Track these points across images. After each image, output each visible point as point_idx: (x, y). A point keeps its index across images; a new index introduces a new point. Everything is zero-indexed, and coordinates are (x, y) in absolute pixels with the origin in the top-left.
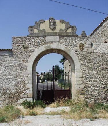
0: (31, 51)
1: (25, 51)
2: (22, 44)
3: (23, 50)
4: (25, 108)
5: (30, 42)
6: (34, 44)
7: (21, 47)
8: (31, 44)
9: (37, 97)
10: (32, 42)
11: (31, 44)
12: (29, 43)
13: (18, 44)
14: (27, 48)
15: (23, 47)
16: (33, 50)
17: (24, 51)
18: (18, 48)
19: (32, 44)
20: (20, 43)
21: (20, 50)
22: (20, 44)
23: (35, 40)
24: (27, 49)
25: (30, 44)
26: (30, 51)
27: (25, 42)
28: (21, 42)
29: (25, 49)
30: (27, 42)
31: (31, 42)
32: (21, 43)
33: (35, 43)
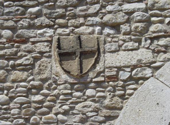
0: (124, 75)
1: (68, 72)
2: (50, 32)
3: (59, 69)
4: (83, 32)
5: (107, 18)
6: (146, 30)
7: (42, 47)
8: (116, 27)
9: (47, 90)
10: (130, 13)
11: (116, 27)
12: (104, 25)
13: (13, 29)
14: (85, 54)
15: (54, 53)
16: (139, 65)
17: (64, 77)
18: (14, 56)
19: (124, 28)
20: (31, 27)
21: (28, 68)
22: (30, 33)
23: (112, 94)
24: (89, 63)
25: (107, 31)
26: (115, 78)
27: (75, 16)
28: (38, 15)
29: (73, 65)
30: (85, 17)
31: (120, 18)
32: (41, 27)
33: (148, 22)
